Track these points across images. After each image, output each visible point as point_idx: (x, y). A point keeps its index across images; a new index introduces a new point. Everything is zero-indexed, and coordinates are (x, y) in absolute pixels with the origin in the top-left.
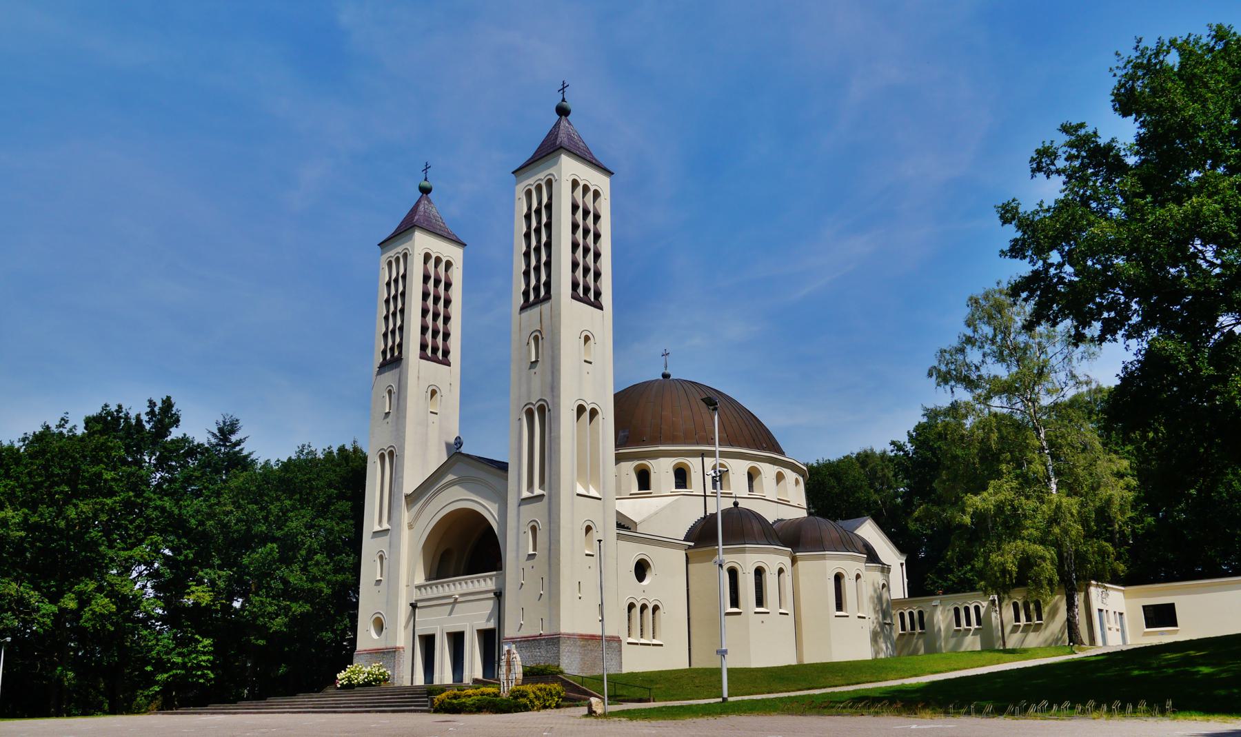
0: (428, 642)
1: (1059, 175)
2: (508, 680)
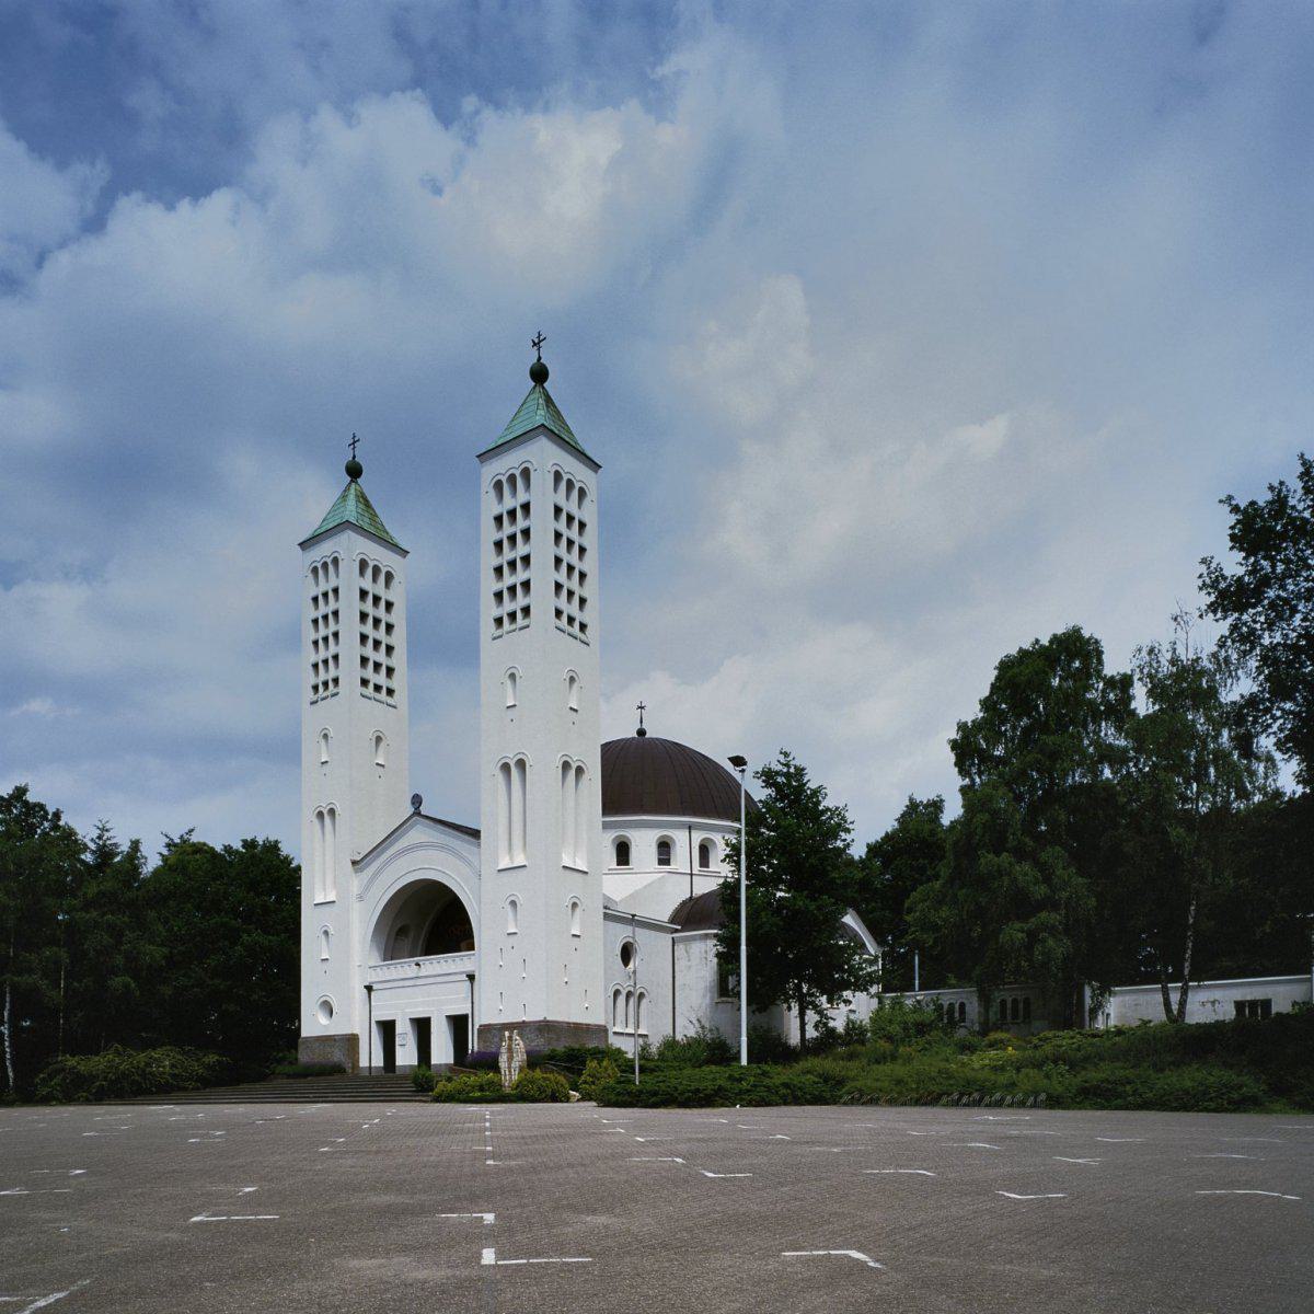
0: (388, 1029)
1: (1301, 476)
2: (509, 1068)
